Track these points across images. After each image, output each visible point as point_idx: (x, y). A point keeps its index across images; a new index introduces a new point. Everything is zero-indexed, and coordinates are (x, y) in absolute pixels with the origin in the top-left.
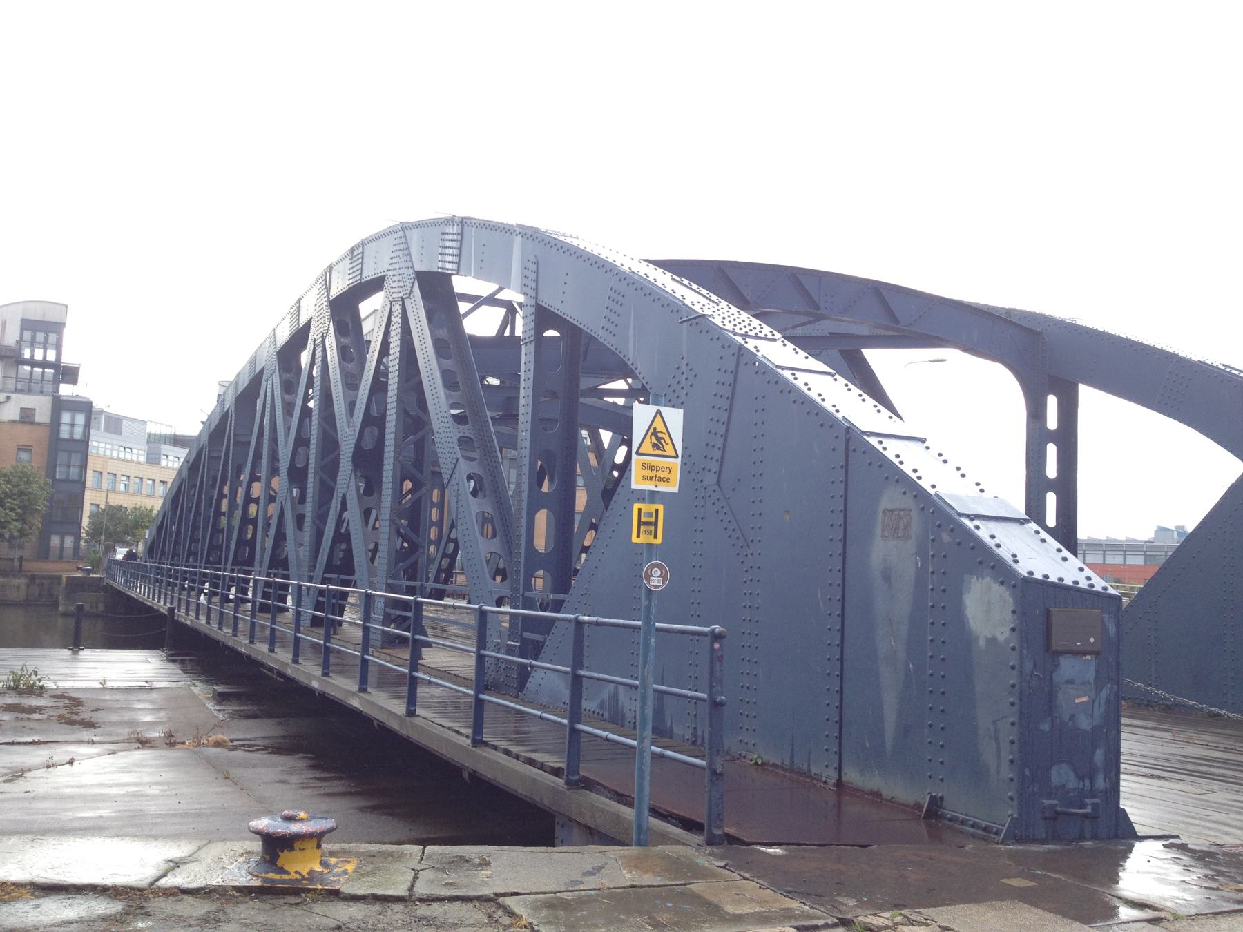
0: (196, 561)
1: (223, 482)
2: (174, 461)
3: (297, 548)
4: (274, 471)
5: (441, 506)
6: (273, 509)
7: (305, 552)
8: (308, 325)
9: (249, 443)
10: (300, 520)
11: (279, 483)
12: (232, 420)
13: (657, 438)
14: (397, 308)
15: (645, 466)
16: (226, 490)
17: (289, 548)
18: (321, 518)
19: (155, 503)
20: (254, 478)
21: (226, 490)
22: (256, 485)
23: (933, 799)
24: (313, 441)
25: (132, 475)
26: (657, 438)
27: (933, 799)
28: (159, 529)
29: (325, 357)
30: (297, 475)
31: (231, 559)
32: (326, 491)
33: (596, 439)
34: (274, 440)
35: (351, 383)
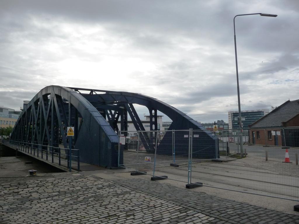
0: (21, 139)
1: (25, 125)
2: (15, 118)
3: (39, 137)
4: (34, 124)
5: (60, 131)
6: (35, 130)
7: (40, 138)
8: (39, 99)
9: (30, 118)
10: (39, 132)
11: (35, 126)
12: (26, 113)
13: (71, 130)
14: (52, 99)
15: (69, 133)
16: (26, 126)
17: (38, 138)
18: (42, 132)
19: (13, 126)
20: (31, 124)
21: (26, 126)
22: (31, 126)
23: (163, 126)
24: (52, 116)
25: (11, 121)
26: (71, 130)
27: (163, 126)
28: (13, 133)
29: (42, 106)
30: (38, 125)
31: (27, 139)
32: (43, 127)
33: (111, 112)
34: (43, 115)
35: (46, 109)
